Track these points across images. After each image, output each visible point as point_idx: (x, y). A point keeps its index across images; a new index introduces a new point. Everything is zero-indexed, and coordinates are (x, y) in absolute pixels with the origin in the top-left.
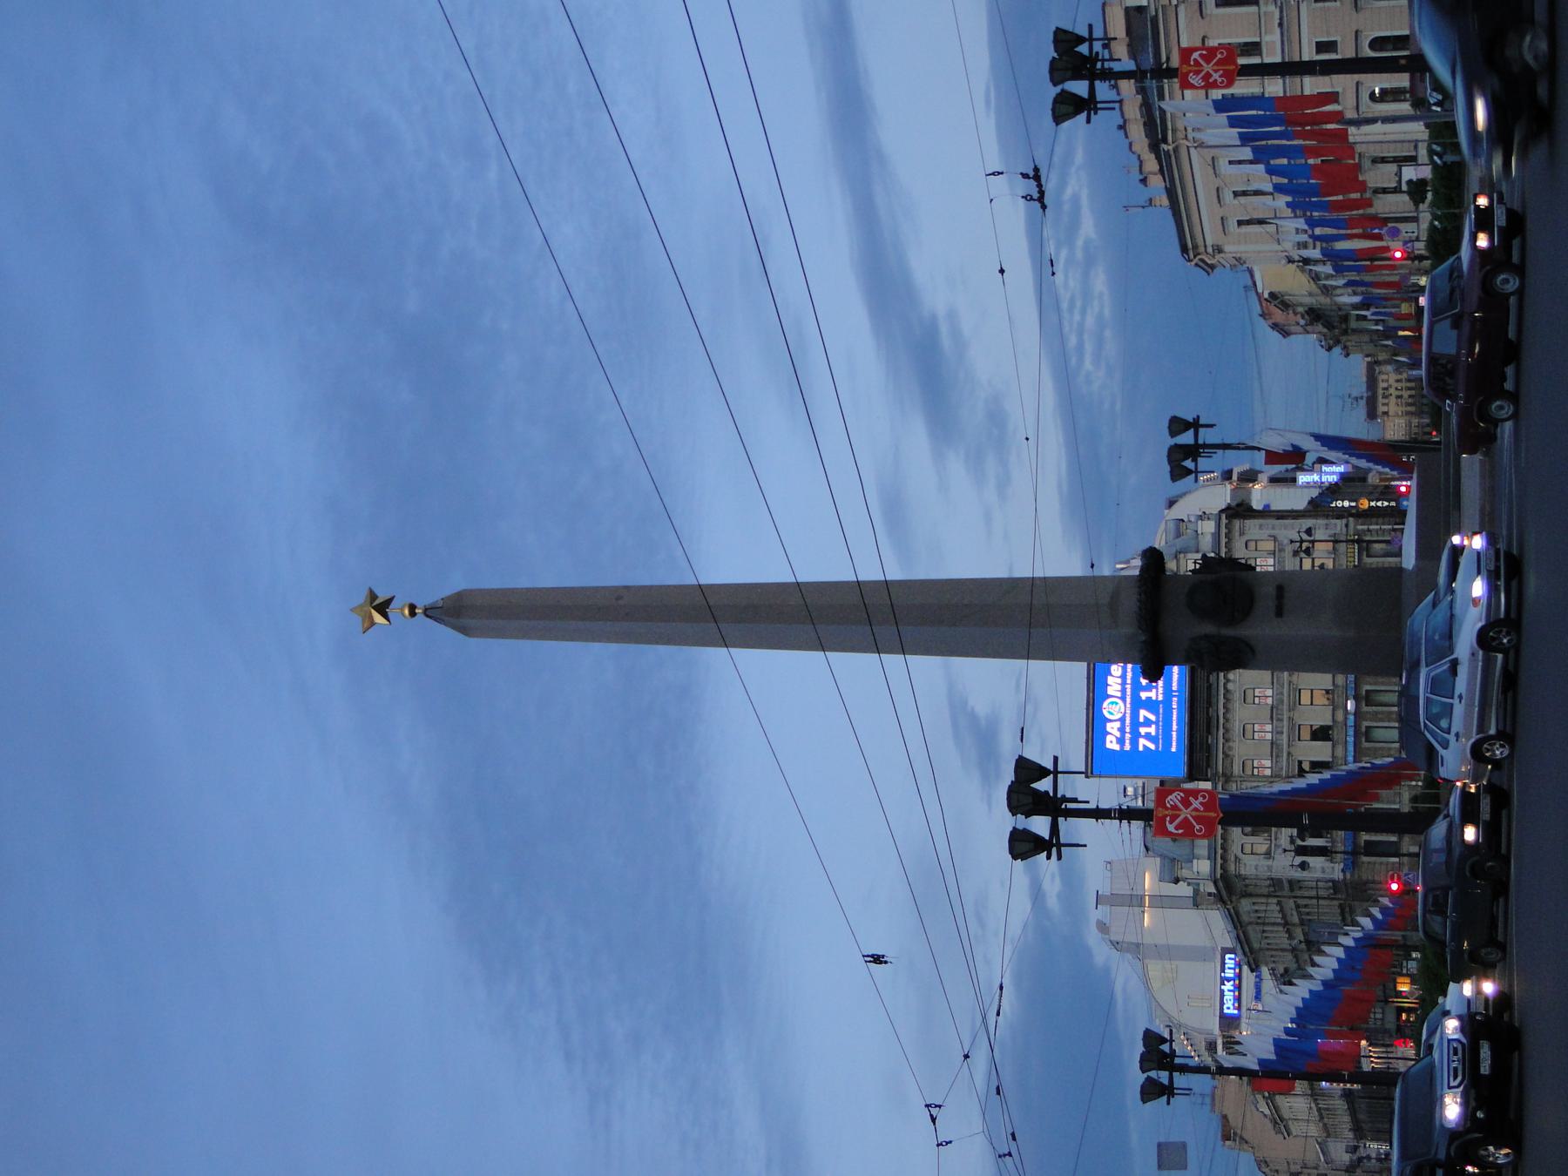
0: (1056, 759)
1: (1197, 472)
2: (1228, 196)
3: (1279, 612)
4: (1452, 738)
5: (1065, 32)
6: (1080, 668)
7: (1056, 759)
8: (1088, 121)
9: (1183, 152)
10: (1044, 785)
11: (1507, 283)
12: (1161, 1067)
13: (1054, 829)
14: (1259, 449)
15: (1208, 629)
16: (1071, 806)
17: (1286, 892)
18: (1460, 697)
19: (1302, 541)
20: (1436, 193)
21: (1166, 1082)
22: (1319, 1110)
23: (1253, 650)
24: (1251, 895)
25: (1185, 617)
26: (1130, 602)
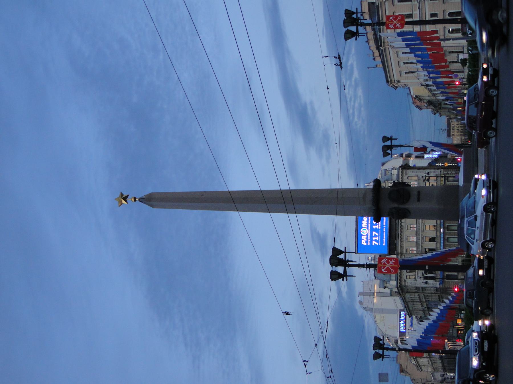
0: (345, 248)
1: (391, 154)
2: (402, 64)
3: (419, 200)
4: (475, 241)
5: (348, 10)
6: (353, 218)
7: (345, 248)
8: (356, 40)
9: (387, 50)
10: (342, 256)
11: (493, 92)
12: (380, 349)
13: (345, 271)
14: (412, 147)
15: (395, 205)
16: (350, 263)
17: (421, 291)
18: (478, 228)
19: (426, 177)
20: (470, 63)
21: (381, 353)
22: (432, 362)
23: (410, 212)
24: (409, 292)
25: (388, 201)
26: (370, 197)
